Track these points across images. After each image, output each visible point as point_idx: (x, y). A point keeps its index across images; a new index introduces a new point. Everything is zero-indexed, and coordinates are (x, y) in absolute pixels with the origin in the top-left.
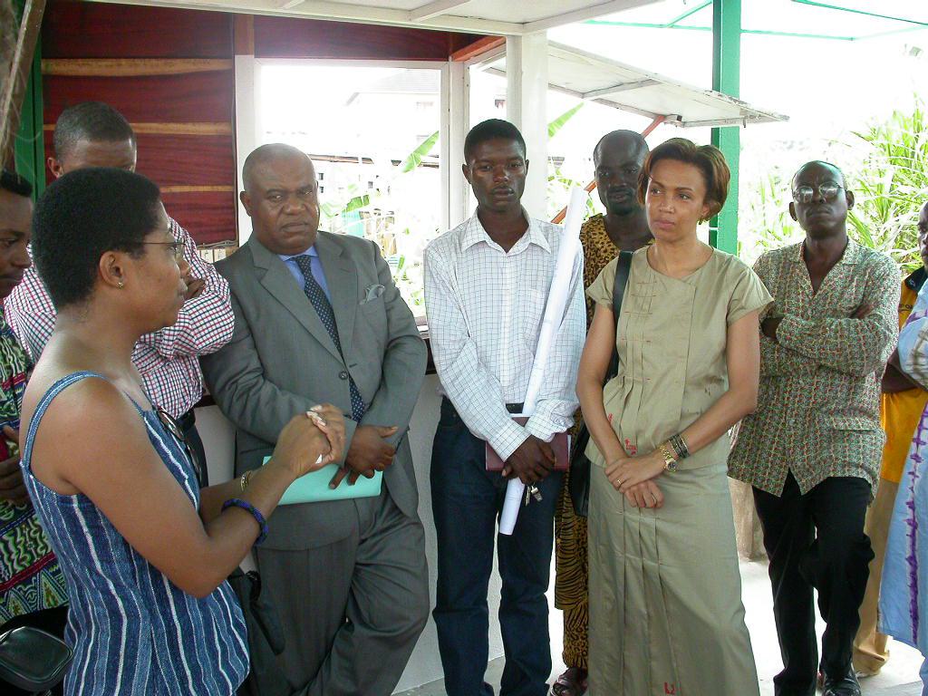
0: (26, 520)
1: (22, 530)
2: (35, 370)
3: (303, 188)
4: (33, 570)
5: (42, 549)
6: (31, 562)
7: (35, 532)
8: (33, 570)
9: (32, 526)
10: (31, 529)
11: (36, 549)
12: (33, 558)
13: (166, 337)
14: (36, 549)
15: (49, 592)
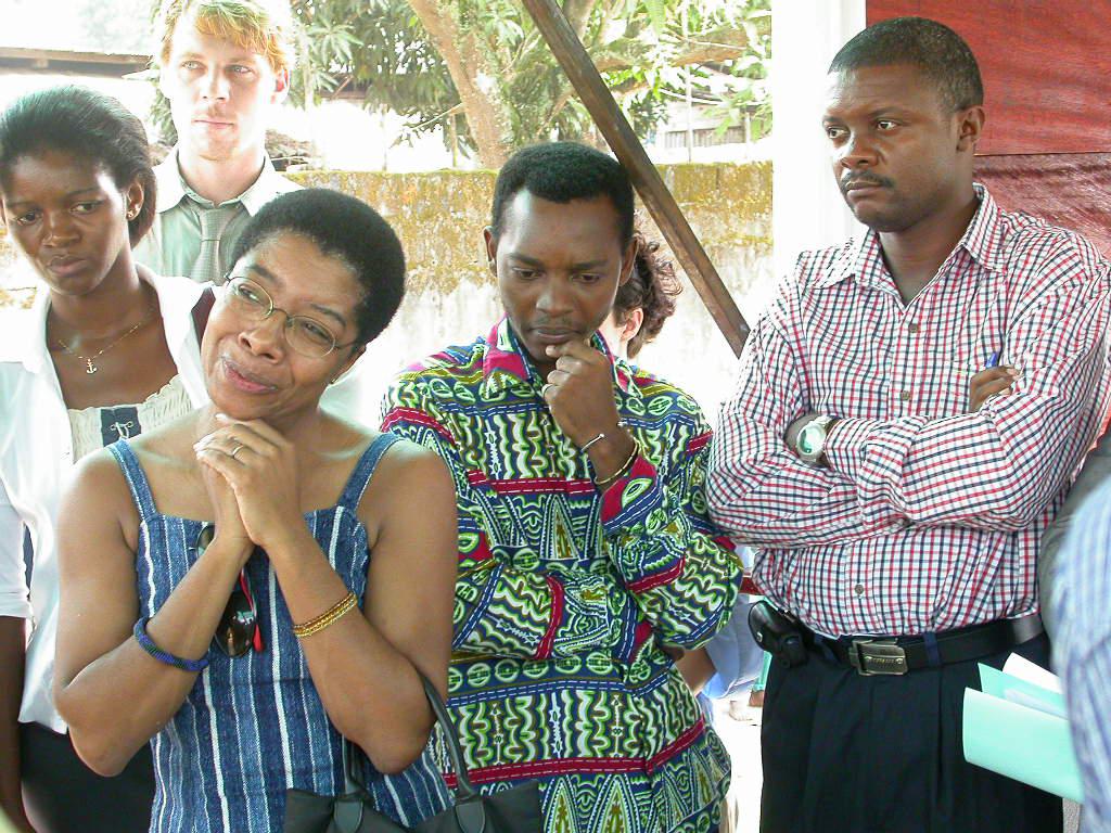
0: (504, 699)
1: (488, 709)
2: (270, 557)
3: (71, 195)
4: (487, 775)
5: (514, 751)
6: (605, 752)
7: (513, 722)
8: (487, 775)
9: (510, 711)
10: (507, 715)
11: (503, 747)
12: (494, 758)
13: (918, 539)
14: (503, 747)
15: (616, 810)
